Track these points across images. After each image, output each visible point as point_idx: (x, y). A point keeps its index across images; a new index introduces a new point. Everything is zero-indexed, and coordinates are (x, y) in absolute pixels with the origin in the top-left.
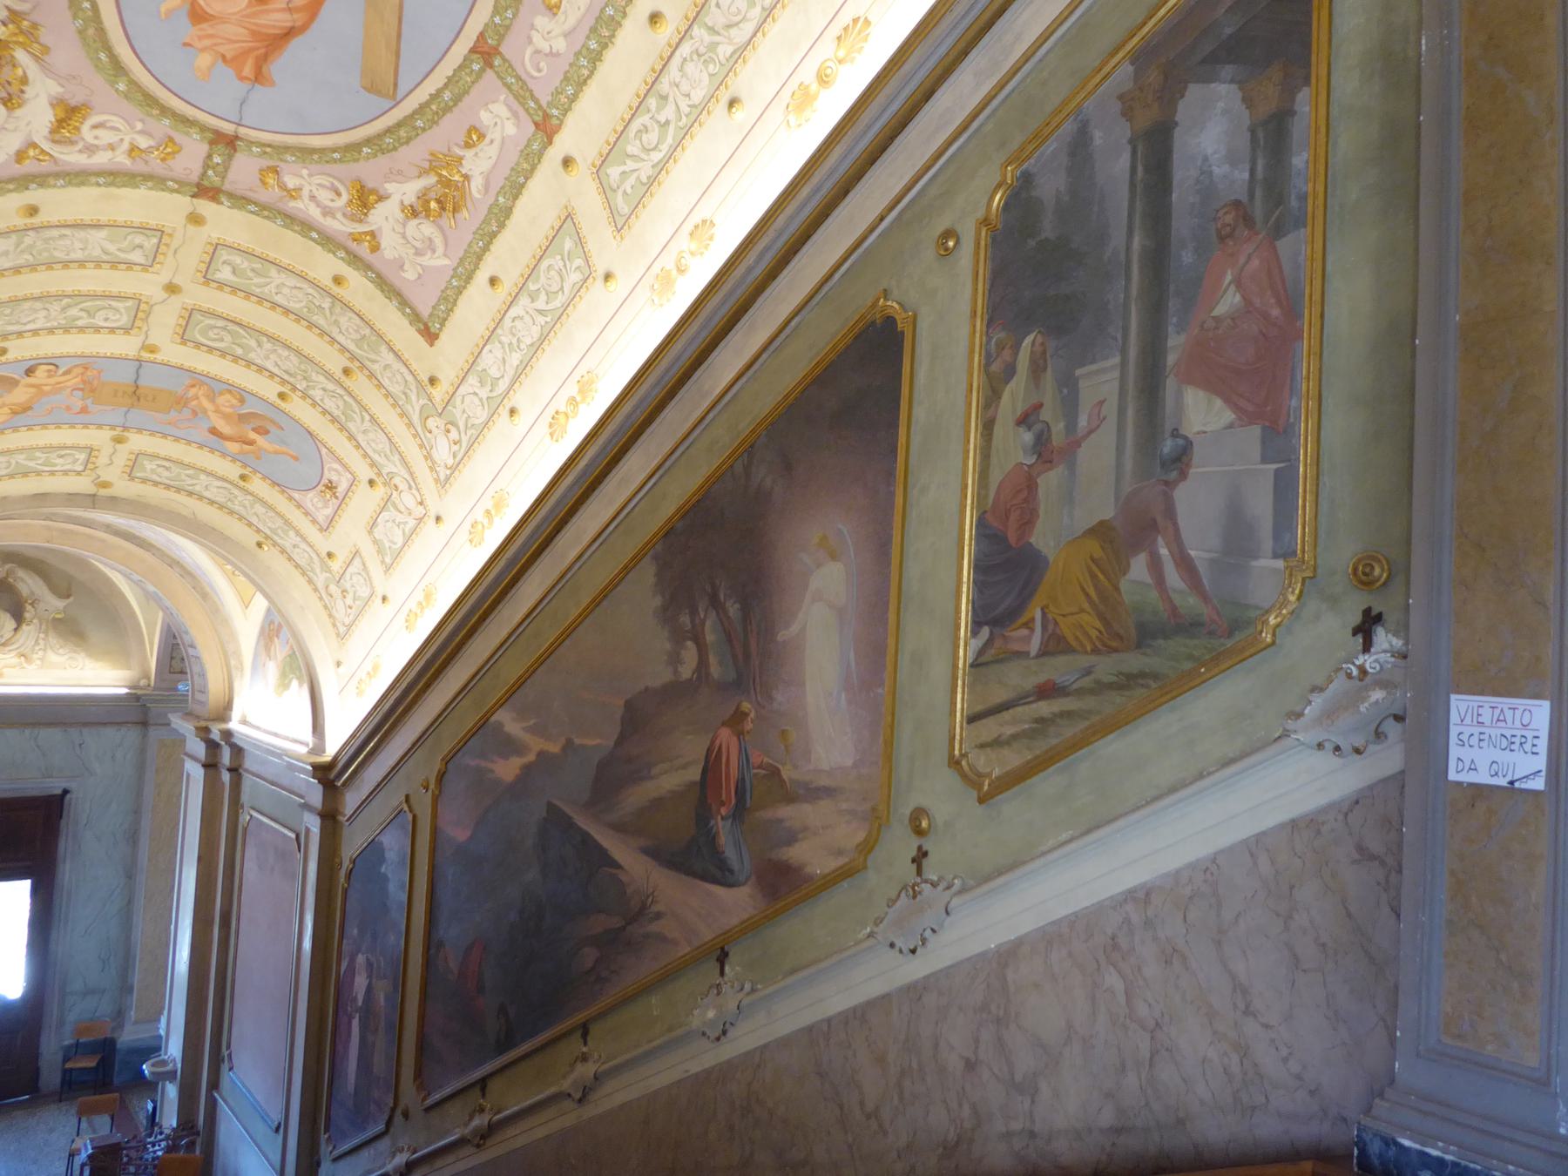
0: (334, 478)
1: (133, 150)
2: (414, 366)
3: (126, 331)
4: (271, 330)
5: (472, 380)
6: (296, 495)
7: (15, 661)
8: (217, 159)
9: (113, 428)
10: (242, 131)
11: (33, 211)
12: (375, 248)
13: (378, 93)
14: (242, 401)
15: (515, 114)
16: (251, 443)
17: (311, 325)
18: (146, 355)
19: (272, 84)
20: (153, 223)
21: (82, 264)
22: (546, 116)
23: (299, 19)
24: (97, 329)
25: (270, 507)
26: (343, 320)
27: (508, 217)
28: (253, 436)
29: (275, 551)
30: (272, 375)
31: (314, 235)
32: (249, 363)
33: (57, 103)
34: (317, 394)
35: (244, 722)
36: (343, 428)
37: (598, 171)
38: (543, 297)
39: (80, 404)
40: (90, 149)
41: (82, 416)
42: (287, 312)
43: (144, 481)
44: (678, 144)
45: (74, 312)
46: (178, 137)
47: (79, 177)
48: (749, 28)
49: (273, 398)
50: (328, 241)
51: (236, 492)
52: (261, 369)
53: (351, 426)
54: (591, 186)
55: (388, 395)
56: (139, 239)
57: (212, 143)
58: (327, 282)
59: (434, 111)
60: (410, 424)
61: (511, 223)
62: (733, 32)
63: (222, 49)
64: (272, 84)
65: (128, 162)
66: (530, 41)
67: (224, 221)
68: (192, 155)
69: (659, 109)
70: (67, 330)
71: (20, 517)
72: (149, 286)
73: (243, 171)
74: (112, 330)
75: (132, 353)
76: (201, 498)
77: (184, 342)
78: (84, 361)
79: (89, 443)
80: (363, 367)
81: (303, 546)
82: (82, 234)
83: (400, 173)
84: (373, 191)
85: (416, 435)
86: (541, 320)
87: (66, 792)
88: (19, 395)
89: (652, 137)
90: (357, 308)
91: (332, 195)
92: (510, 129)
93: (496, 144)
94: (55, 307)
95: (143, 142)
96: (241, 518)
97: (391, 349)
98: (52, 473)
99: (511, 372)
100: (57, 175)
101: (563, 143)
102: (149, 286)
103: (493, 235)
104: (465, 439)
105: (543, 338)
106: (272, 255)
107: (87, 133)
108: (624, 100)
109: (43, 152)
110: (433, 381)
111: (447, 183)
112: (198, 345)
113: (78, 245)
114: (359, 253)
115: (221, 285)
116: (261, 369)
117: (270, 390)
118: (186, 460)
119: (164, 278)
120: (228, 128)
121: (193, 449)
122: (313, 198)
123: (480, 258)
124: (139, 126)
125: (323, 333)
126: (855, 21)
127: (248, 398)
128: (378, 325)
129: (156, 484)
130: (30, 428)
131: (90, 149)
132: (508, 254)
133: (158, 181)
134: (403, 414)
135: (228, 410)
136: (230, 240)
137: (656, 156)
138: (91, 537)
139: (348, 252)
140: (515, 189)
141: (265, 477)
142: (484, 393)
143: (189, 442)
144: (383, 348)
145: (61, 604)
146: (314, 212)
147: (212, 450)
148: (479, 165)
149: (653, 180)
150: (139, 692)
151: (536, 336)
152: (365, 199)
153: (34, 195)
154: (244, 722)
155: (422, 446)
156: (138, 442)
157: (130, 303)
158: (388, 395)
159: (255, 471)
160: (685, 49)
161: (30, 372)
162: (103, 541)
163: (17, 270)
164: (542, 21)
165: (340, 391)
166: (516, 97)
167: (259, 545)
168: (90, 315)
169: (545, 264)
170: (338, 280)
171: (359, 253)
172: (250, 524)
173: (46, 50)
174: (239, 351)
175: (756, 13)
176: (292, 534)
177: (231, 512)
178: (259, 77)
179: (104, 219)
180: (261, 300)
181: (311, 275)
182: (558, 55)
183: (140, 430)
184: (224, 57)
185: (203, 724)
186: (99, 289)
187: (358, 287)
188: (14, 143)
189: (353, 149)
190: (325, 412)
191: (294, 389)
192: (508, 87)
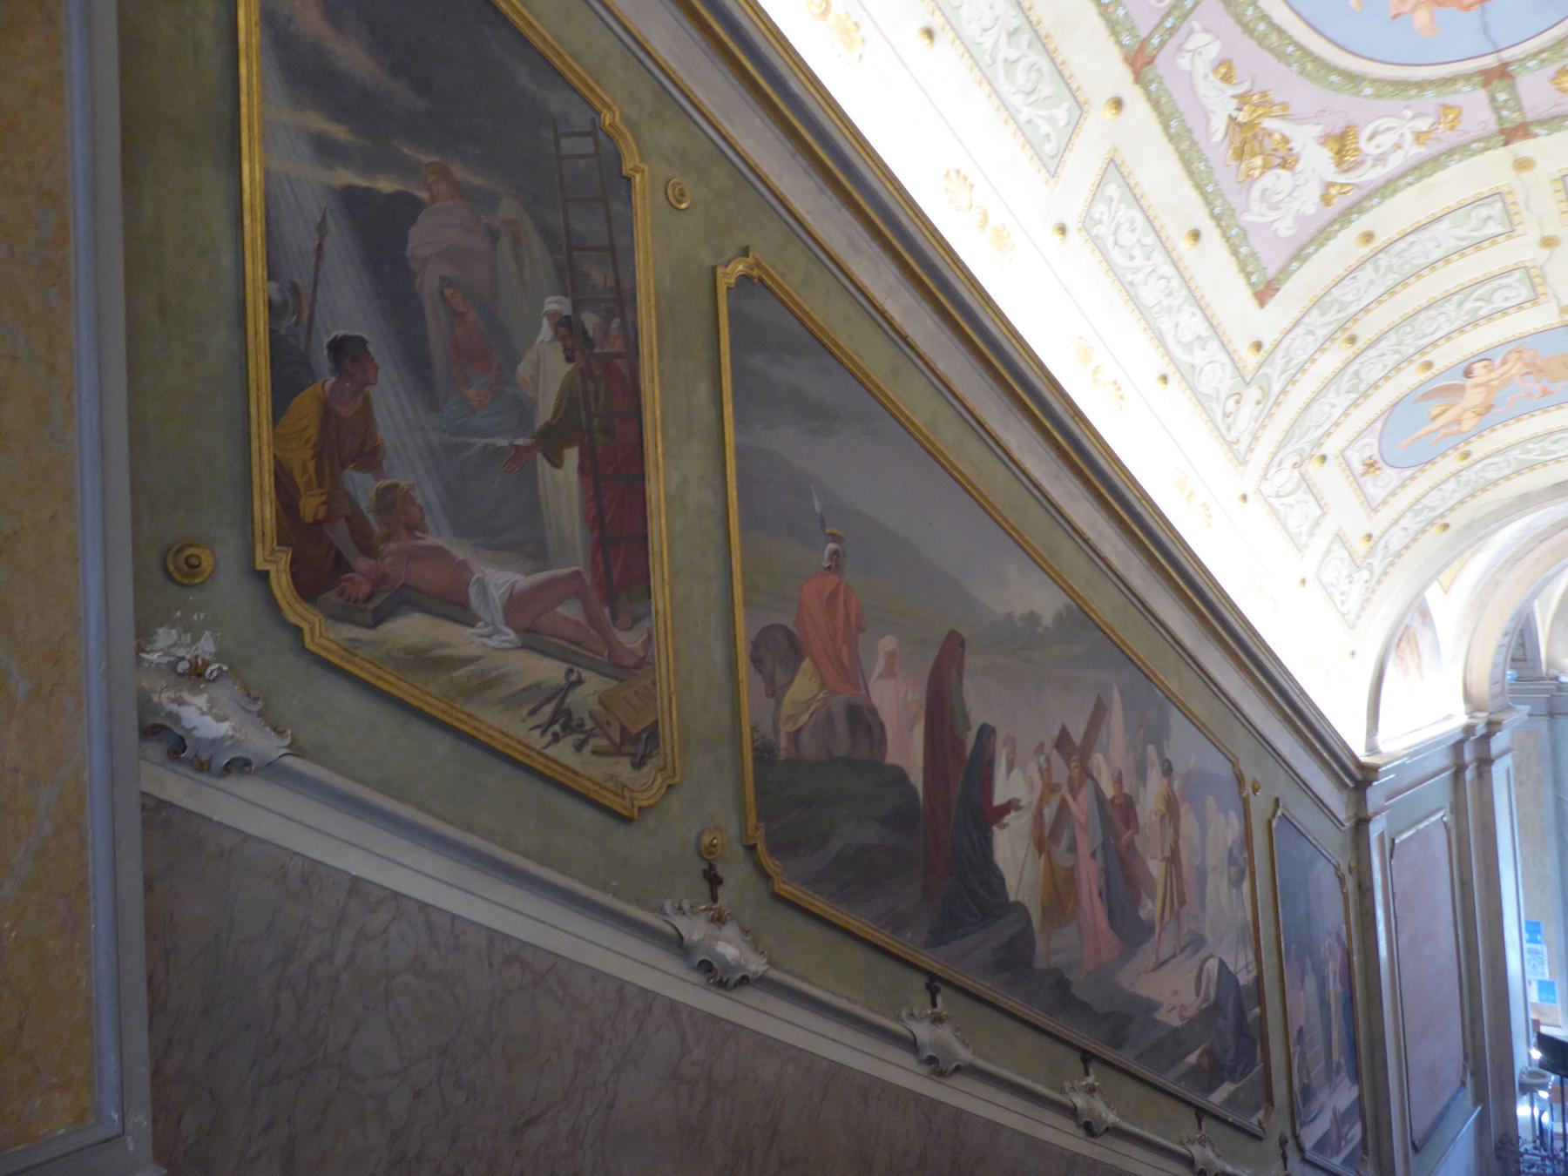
1: (1419, 137)
3: (1534, 300)
8: (1502, 97)
10: (1506, 55)
11: (1368, 237)
20: (1486, 190)
21: (1446, 259)
24: (1504, 312)
33: (1325, 140)
40: (1381, 159)
45: (1469, 305)
46: (1450, 100)
47: (1389, 187)
56: (1483, 212)
57: (1485, 84)
70: (1475, 323)
72: (1525, 249)
74: (1520, 307)
88: (1474, 397)
94: (1450, 307)
95: (1423, 124)
100: (1368, 197)
102: (1525, 249)
109: (1343, 185)
120: (1490, 61)
130: (1505, 423)
131: (1381, 159)
153: (1360, 224)
157: (1518, 274)
161: (1468, 373)
163: (1391, 291)
173: (1285, 106)
179: (1438, 211)
188: (1313, 193)
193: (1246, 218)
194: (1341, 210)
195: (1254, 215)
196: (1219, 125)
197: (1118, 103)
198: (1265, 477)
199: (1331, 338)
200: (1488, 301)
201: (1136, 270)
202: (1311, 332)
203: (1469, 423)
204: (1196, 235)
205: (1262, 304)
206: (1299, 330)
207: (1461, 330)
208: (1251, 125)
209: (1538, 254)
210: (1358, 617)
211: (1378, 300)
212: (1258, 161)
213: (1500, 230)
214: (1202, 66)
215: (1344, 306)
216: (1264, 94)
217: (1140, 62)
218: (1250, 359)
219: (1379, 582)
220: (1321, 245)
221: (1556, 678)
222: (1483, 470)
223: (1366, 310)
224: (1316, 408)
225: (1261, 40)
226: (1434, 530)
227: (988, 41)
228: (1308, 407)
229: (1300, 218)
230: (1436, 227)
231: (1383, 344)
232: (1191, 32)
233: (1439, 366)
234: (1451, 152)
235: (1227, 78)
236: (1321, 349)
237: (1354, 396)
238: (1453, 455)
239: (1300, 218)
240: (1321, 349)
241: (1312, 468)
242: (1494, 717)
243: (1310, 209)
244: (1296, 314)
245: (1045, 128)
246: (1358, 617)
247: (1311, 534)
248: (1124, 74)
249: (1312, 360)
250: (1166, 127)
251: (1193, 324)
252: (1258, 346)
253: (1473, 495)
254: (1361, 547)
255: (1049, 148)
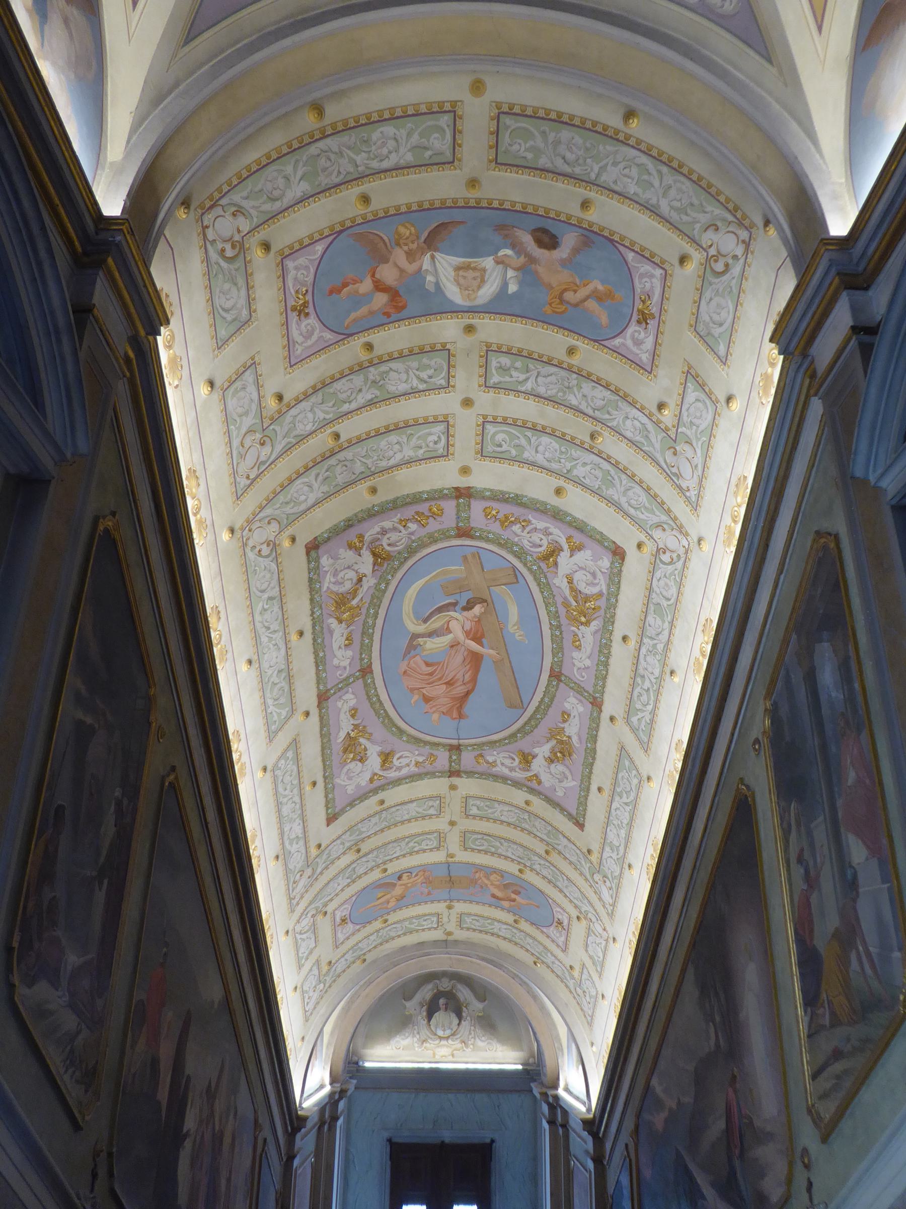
0: (560, 917)
1: (417, 764)
2: (578, 844)
3: (438, 849)
4: (505, 836)
5: (607, 849)
6: (545, 930)
7: (459, 1046)
8: (454, 757)
9: (445, 901)
10: (461, 741)
11: (382, 802)
12: (540, 783)
13: (515, 707)
14: (502, 876)
15: (581, 701)
16: (514, 900)
17: (523, 830)
18: (450, 860)
19: (468, 717)
20: (435, 794)
21: (409, 821)
22: (595, 698)
23: (470, 686)
24: (424, 851)
25: (534, 938)
26: (537, 824)
27: (595, 753)
28: (513, 896)
29: (544, 966)
30: (513, 860)
31: (509, 782)
32: (500, 855)
33: (380, 754)
34: (537, 867)
35: (567, 1089)
36: (555, 886)
37: (628, 721)
38: (625, 795)
39: (426, 891)
40: (399, 769)
41: (429, 898)
42: (509, 824)
43: (468, 929)
44: (657, 700)
45: (411, 844)
46: (435, 753)
47: (398, 782)
48: (666, 633)
49: (517, 873)
50: (517, 784)
51: (514, 931)
52: (506, 858)
53: (559, 884)
54: (627, 729)
55: (571, 863)
56: (431, 803)
57: (449, 751)
58: (523, 805)
59: (543, 708)
60: (586, 880)
61: (597, 756)
62: (660, 636)
63: (442, 709)
64: (468, 717)
65: (416, 769)
66: (574, 665)
67: (467, 786)
68: (443, 759)
69: (643, 683)
70: (411, 854)
71: (435, 953)
72: (441, 824)
73: (467, 759)
74: (431, 850)
75: (444, 860)
76: (499, 936)
77: (466, 849)
78: (422, 868)
79: (436, 911)
80: (554, 848)
81: (557, 962)
82: (406, 807)
83: (538, 742)
84: (529, 754)
85: (591, 886)
86: (628, 808)
87: (493, 1141)
88: (398, 891)
89: (644, 698)
90: (541, 816)
91: (510, 761)
92: (581, 709)
93: (577, 718)
94: (403, 844)
95: (421, 759)
96: (522, 947)
97: (564, 836)
98: (423, 930)
99: (623, 842)
100: (388, 784)
101: (608, 708)
102: (441, 824)
103: (592, 764)
104: (614, 886)
105: (632, 819)
106: (493, 797)
107: (396, 762)
108: (626, 681)
109: (380, 776)
110: (589, 851)
111: (561, 742)
112: (473, 850)
113: (405, 812)
114: (533, 786)
115: (474, 817)
116: (506, 858)
117: (513, 868)
118: (486, 915)
119: (447, 818)
120: (455, 742)
121: (487, 908)
122: (502, 764)
123: (590, 778)
124: (417, 753)
125: (530, 833)
126: (707, 620)
127: (505, 875)
128: (555, 824)
129: (474, 930)
130: (407, 907)
131: (399, 769)
132: (602, 774)
133: (432, 774)
134: (581, 874)
135: (497, 883)
136: (471, 794)
137: (650, 708)
138: (471, 962)
139: (528, 787)
140: (594, 738)
141: (526, 920)
142: (615, 857)
143: (484, 904)
144: (561, 836)
145: (480, 1006)
146: (506, 771)
147: (496, 907)
148: (572, 729)
149: (652, 721)
150: (529, 1068)
151: (628, 818)
152: (527, 759)
153: (381, 795)
154: (567, 1089)
155: (595, 892)
156: (460, 907)
157: (435, 835)
158: (571, 863)
159: (521, 917)
160: (643, 651)
161: (400, 878)
162: (479, 964)
163: (382, 830)
164: (575, 654)
165: (547, 864)
166: (578, 692)
167: (535, 963)
168: (420, 844)
169: (620, 776)
170: (527, 803)
171: (533, 786)
172: (527, 950)
173: (371, 734)
174: (493, 850)
175: (666, 625)
176: (549, 955)
177: (516, 944)
178: (461, 716)
179: (413, 798)
180: (495, 821)
181: (515, 803)
182: (588, 667)
183: (458, 901)
184: (444, 713)
185: (544, 1090)
186: (420, 831)
187: (538, 805)
188: (367, 776)
189: (513, 736)
190: (544, 877)
191: (525, 866)
192: (572, 688)
193: (337, 781)
194: (377, 786)
195: (340, 781)
196: (342, 735)
197: (307, 714)
198: (298, 922)
199: (350, 848)
200: (420, 844)
201: (285, 796)
202: (343, 844)
203: (392, 904)
204: (314, 784)
205: (328, 825)
206: (339, 842)
207: (404, 856)
208: (355, 739)
209: (447, 828)
210: (311, 1014)
211: (375, 834)
212: (351, 756)
213: (435, 813)
214: (346, 708)
215: (361, 833)
216: (365, 727)
217: (323, 698)
218: (314, 852)
219: (326, 991)
220: (362, 801)
221: (357, 1063)
222: (390, 930)
223: (369, 837)
224: (331, 884)
225: (372, 704)
226: (358, 962)
227: (270, 672)
228: (329, 882)
229: (358, 786)
230: (410, 805)
231: (370, 856)
232: (347, 692)
233: (389, 872)
234: (426, 774)
235: (353, 716)
236: (344, 853)
237: (349, 880)
238: (380, 920)
239: (358, 786)
240: (344, 853)
241: (320, 917)
242: (344, 1087)
243: (363, 783)
244: (340, 833)
245: (276, 718)
246: (311, 1014)
247: (307, 959)
248: (314, 701)
249: (338, 858)
250: (321, 730)
251: (298, 830)
252: (319, 846)
253: (381, 944)
254: (325, 968)
255: (273, 728)
